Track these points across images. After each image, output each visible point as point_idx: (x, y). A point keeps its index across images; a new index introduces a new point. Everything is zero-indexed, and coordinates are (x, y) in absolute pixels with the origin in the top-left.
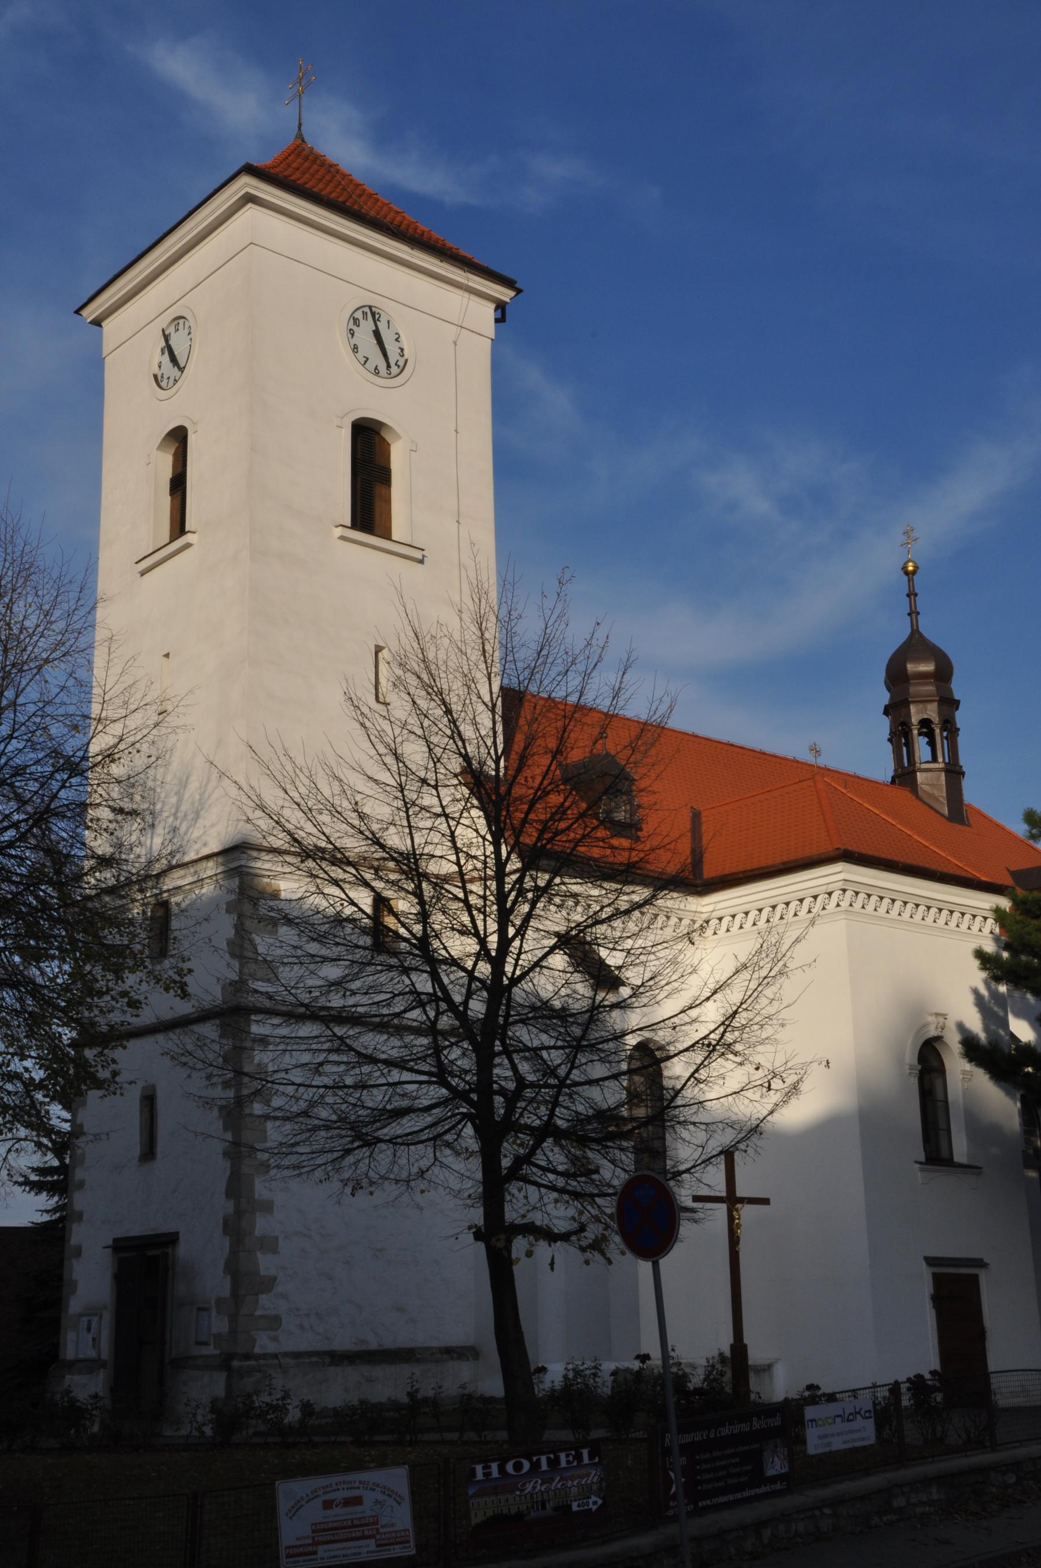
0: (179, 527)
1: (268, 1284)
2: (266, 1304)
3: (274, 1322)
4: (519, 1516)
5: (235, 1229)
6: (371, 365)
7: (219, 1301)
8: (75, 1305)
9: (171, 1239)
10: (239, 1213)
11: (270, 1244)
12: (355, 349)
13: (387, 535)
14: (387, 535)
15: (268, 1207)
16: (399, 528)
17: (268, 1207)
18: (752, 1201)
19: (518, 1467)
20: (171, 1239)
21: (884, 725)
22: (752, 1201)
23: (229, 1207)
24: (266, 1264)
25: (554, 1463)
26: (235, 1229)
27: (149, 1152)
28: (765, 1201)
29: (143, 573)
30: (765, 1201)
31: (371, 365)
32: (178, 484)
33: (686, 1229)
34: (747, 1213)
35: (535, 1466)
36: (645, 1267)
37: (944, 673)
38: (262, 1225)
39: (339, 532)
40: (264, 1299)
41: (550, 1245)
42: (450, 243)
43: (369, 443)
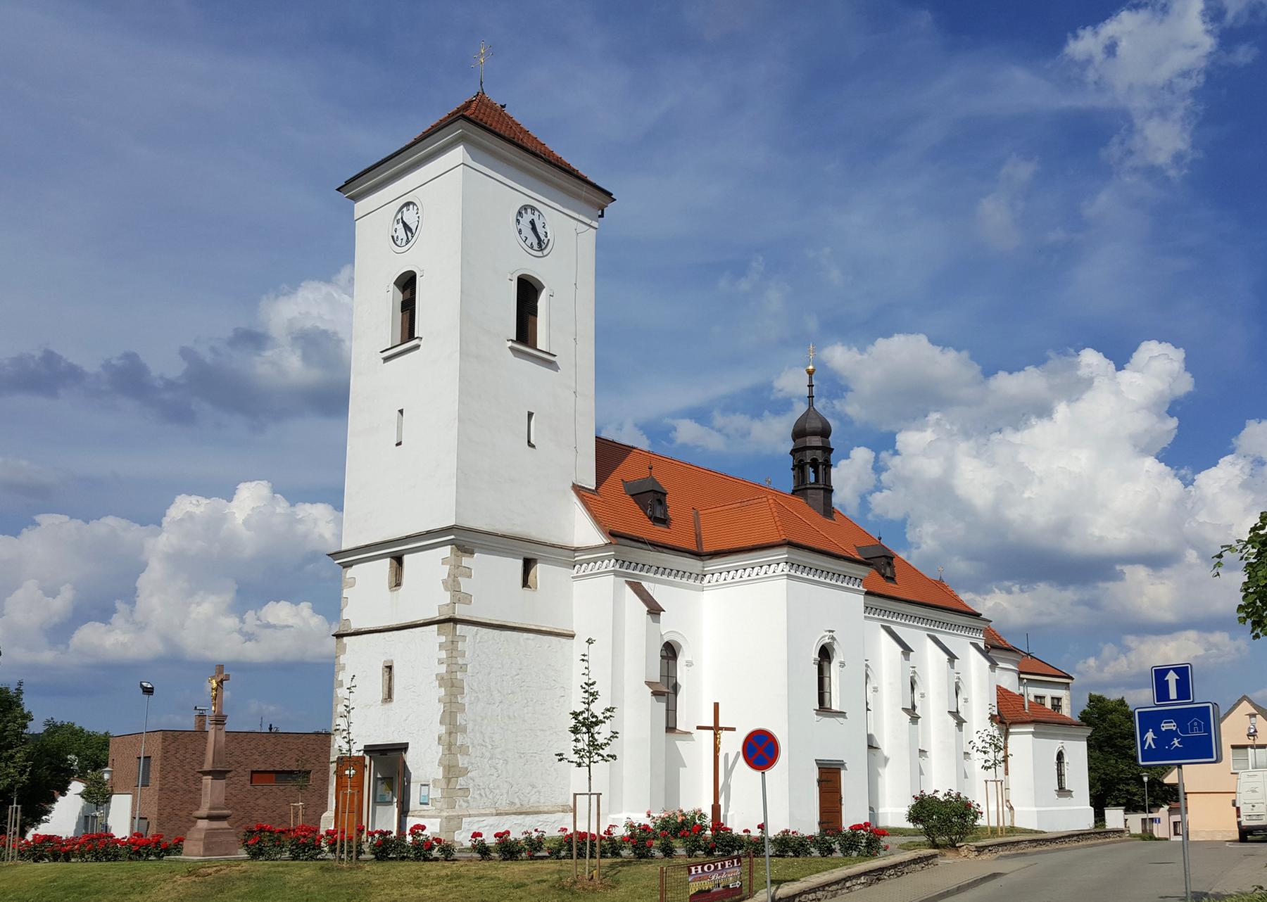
0: (409, 331)
1: (465, 772)
4: (709, 891)
6: (528, 242)
7: (435, 781)
9: (403, 747)
12: (520, 232)
14: (534, 346)
16: (541, 344)
18: (727, 729)
19: (709, 868)
20: (403, 747)
21: (790, 461)
22: (727, 729)
25: (723, 866)
27: (389, 697)
28: (733, 729)
29: (386, 359)
30: (733, 729)
31: (528, 242)
32: (408, 307)
33: (740, 749)
34: (724, 735)
35: (716, 867)
36: (759, 773)
37: (825, 432)
39: (510, 344)
41: (19, 692)
42: (574, 166)
43: (528, 291)
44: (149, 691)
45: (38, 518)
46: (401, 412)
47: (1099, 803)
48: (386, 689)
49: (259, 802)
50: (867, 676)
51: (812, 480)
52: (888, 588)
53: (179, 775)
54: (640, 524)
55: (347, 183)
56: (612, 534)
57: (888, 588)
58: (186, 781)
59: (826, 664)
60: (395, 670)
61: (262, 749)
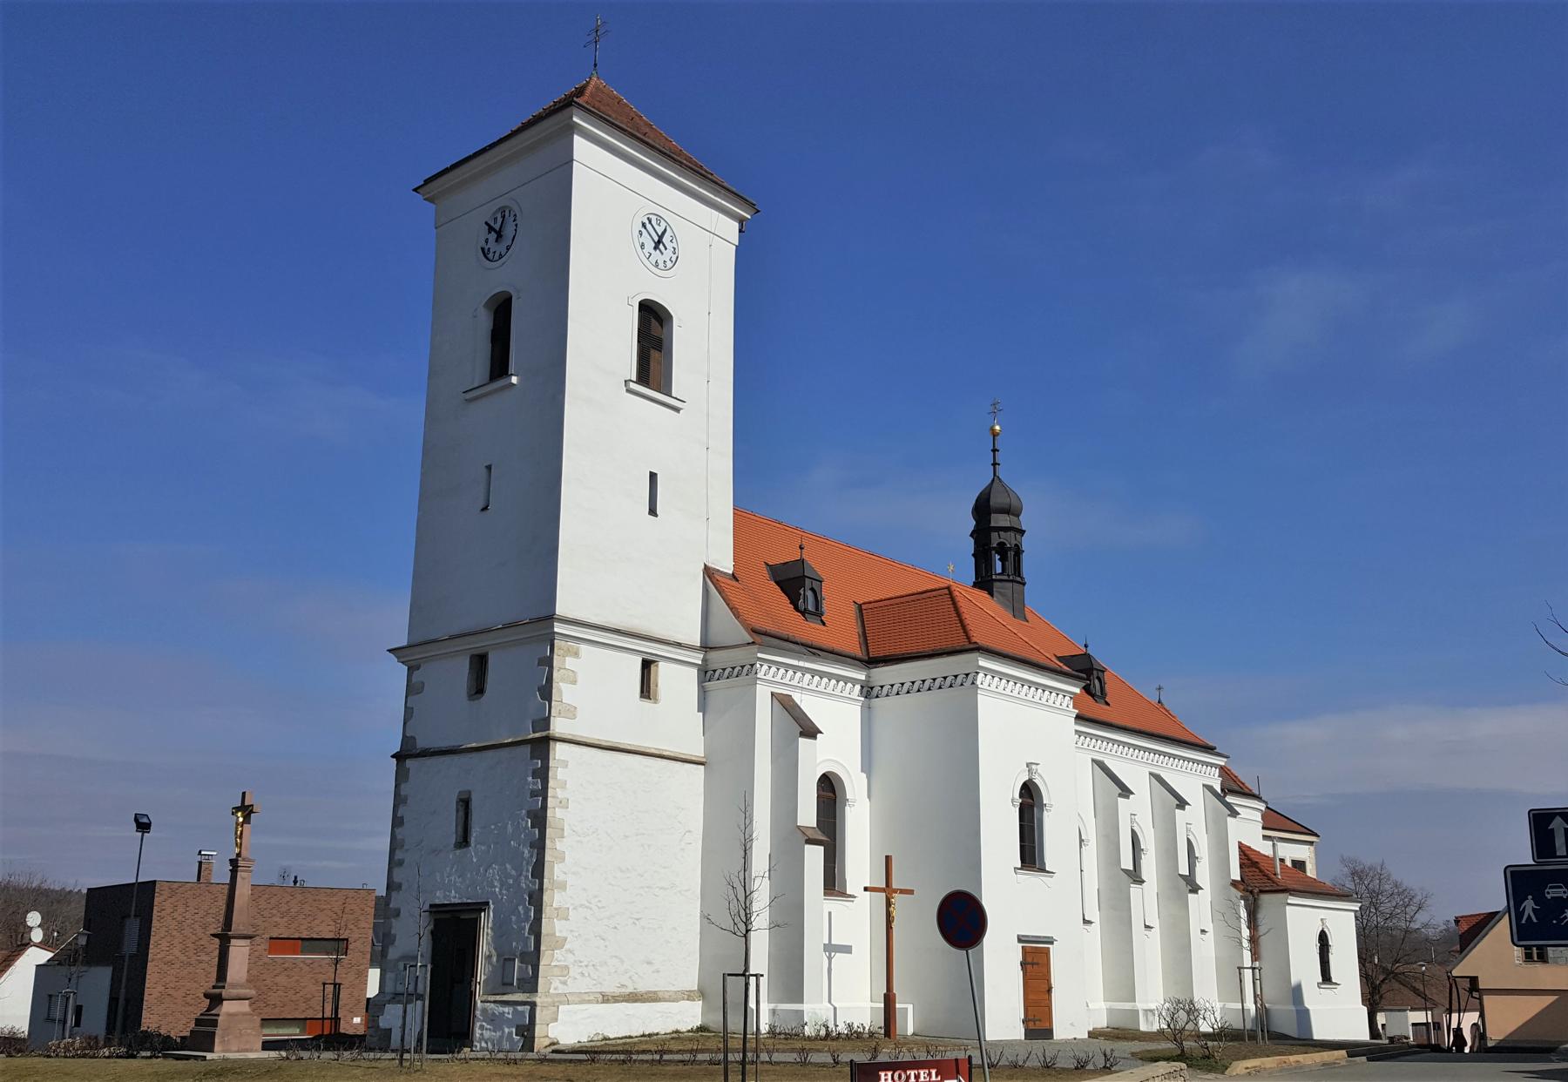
12: (642, 246)
18: (903, 892)
22: (903, 892)
44: (143, 826)
45: (1294, 981)
46: (489, 468)
47: (1374, 999)
48: (460, 829)
49: (278, 979)
50: (1081, 841)
51: (999, 570)
52: (1097, 710)
53: (176, 942)
54: (779, 611)
55: (427, 182)
56: (755, 631)
57: (1097, 710)
58: (184, 951)
59: (654, 354)
60: (474, 804)
61: (284, 908)
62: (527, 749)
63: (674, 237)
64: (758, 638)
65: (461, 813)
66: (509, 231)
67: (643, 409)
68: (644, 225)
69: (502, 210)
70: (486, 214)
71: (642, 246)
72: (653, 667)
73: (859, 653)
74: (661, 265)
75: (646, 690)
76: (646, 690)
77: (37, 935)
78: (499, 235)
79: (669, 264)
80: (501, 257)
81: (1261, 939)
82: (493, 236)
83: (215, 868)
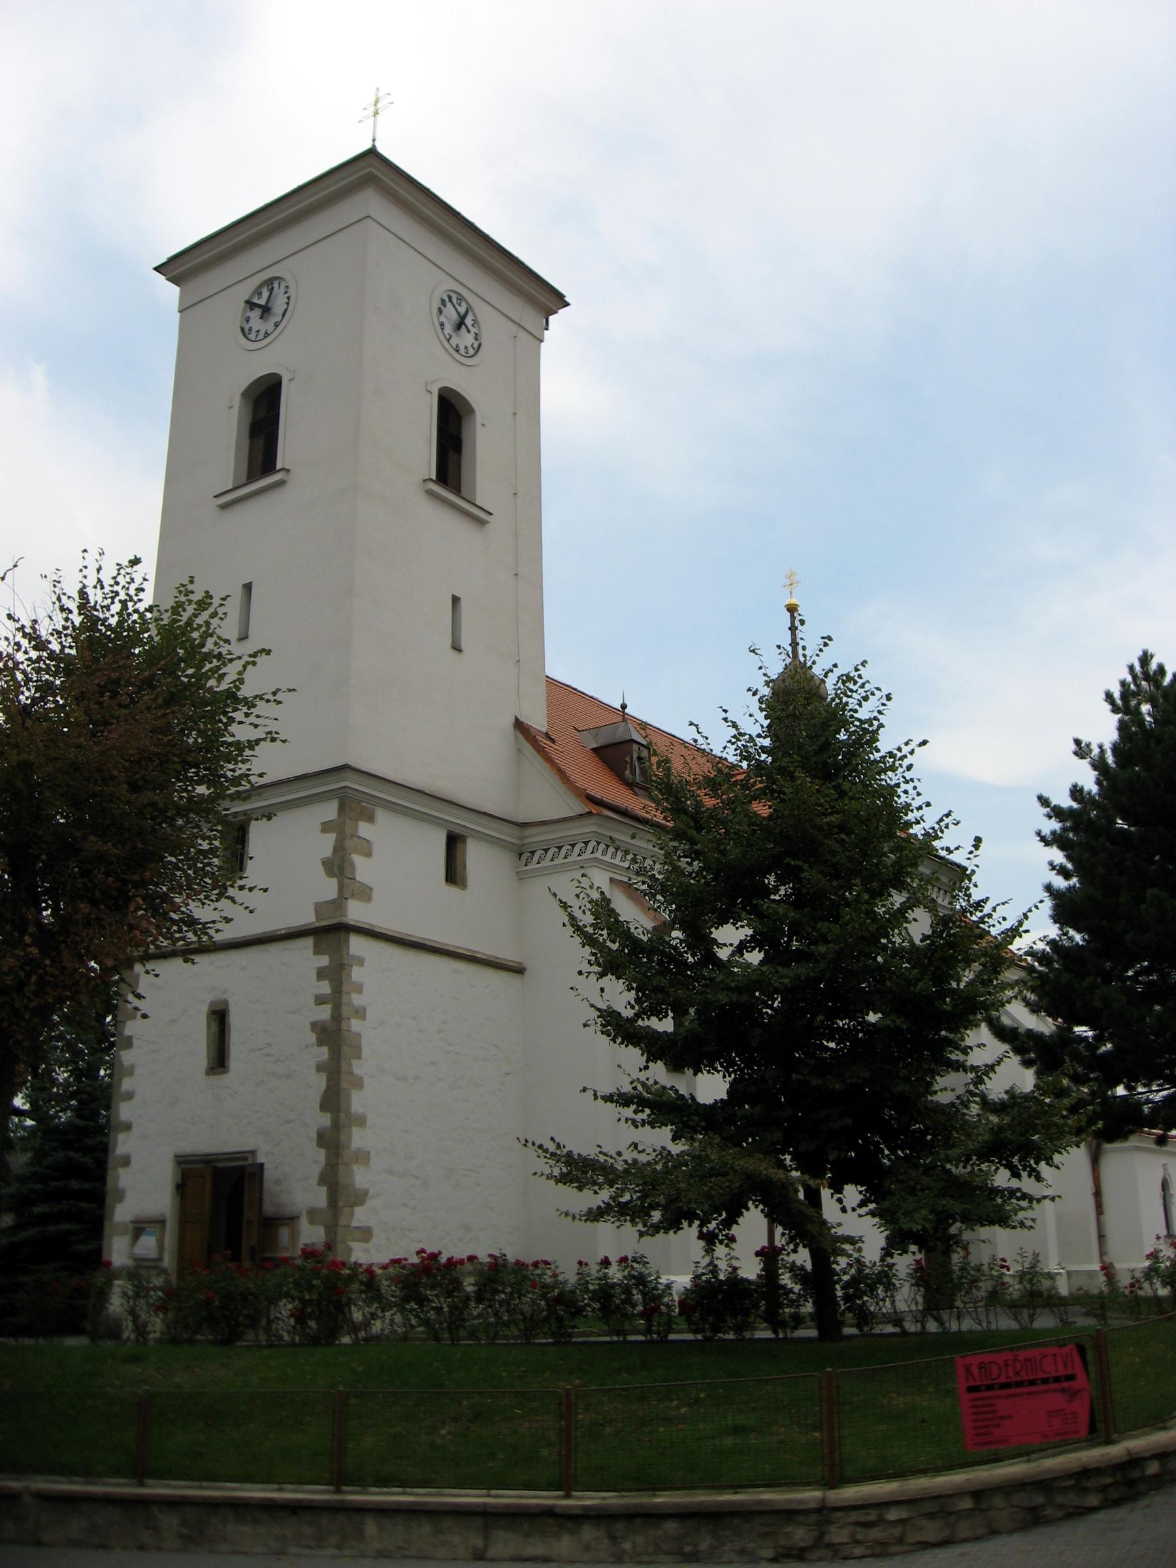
1: (360, 1198)
2: (361, 1216)
3: (366, 1234)
5: (332, 1141)
7: (313, 1214)
8: (122, 1213)
10: (336, 1125)
11: (363, 1157)
12: (442, 325)
13: (457, 490)
15: (361, 1121)
17: (361, 1121)
23: (325, 1120)
24: (361, 1177)
26: (332, 1141)
38: (358, 1139)
40: (357, 1210)
60: (235, 1020)
62: (309, 942)
63: (475, 322)
64: (594, 809)
65: (215, 1027)
66: (279, 305)
67: (436, 522)
68: (443, 301)
69: (270, 283)
70: (245, 291)
71: (442, 325)
72: (459, 846)
73: (357, 945)
74: (462, 351)
75: (454, 874)
76: (454, 874)
77: (609, 944)
78: (266, 310)
79: (471, 352)
80: (267, 335)
81: (709, 1251)
82: (258, 312)
83: (322, 965)
